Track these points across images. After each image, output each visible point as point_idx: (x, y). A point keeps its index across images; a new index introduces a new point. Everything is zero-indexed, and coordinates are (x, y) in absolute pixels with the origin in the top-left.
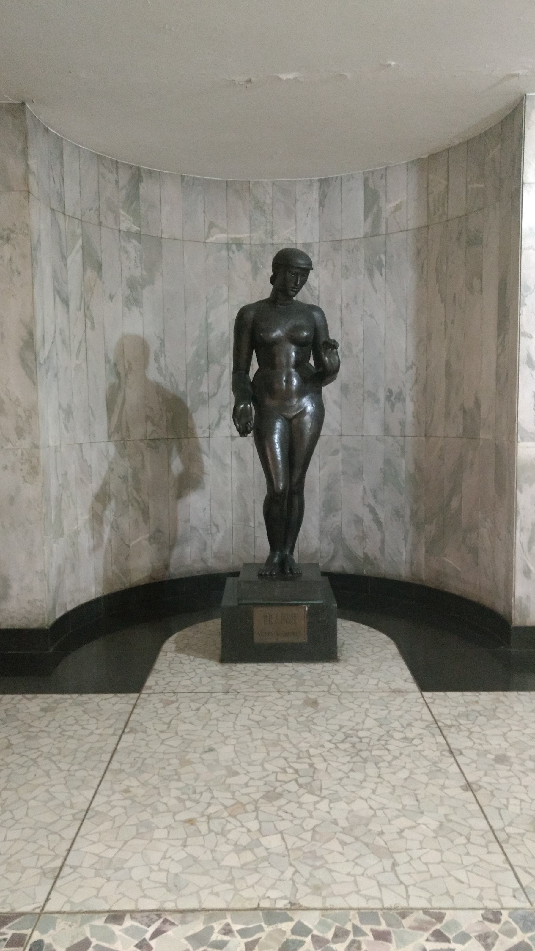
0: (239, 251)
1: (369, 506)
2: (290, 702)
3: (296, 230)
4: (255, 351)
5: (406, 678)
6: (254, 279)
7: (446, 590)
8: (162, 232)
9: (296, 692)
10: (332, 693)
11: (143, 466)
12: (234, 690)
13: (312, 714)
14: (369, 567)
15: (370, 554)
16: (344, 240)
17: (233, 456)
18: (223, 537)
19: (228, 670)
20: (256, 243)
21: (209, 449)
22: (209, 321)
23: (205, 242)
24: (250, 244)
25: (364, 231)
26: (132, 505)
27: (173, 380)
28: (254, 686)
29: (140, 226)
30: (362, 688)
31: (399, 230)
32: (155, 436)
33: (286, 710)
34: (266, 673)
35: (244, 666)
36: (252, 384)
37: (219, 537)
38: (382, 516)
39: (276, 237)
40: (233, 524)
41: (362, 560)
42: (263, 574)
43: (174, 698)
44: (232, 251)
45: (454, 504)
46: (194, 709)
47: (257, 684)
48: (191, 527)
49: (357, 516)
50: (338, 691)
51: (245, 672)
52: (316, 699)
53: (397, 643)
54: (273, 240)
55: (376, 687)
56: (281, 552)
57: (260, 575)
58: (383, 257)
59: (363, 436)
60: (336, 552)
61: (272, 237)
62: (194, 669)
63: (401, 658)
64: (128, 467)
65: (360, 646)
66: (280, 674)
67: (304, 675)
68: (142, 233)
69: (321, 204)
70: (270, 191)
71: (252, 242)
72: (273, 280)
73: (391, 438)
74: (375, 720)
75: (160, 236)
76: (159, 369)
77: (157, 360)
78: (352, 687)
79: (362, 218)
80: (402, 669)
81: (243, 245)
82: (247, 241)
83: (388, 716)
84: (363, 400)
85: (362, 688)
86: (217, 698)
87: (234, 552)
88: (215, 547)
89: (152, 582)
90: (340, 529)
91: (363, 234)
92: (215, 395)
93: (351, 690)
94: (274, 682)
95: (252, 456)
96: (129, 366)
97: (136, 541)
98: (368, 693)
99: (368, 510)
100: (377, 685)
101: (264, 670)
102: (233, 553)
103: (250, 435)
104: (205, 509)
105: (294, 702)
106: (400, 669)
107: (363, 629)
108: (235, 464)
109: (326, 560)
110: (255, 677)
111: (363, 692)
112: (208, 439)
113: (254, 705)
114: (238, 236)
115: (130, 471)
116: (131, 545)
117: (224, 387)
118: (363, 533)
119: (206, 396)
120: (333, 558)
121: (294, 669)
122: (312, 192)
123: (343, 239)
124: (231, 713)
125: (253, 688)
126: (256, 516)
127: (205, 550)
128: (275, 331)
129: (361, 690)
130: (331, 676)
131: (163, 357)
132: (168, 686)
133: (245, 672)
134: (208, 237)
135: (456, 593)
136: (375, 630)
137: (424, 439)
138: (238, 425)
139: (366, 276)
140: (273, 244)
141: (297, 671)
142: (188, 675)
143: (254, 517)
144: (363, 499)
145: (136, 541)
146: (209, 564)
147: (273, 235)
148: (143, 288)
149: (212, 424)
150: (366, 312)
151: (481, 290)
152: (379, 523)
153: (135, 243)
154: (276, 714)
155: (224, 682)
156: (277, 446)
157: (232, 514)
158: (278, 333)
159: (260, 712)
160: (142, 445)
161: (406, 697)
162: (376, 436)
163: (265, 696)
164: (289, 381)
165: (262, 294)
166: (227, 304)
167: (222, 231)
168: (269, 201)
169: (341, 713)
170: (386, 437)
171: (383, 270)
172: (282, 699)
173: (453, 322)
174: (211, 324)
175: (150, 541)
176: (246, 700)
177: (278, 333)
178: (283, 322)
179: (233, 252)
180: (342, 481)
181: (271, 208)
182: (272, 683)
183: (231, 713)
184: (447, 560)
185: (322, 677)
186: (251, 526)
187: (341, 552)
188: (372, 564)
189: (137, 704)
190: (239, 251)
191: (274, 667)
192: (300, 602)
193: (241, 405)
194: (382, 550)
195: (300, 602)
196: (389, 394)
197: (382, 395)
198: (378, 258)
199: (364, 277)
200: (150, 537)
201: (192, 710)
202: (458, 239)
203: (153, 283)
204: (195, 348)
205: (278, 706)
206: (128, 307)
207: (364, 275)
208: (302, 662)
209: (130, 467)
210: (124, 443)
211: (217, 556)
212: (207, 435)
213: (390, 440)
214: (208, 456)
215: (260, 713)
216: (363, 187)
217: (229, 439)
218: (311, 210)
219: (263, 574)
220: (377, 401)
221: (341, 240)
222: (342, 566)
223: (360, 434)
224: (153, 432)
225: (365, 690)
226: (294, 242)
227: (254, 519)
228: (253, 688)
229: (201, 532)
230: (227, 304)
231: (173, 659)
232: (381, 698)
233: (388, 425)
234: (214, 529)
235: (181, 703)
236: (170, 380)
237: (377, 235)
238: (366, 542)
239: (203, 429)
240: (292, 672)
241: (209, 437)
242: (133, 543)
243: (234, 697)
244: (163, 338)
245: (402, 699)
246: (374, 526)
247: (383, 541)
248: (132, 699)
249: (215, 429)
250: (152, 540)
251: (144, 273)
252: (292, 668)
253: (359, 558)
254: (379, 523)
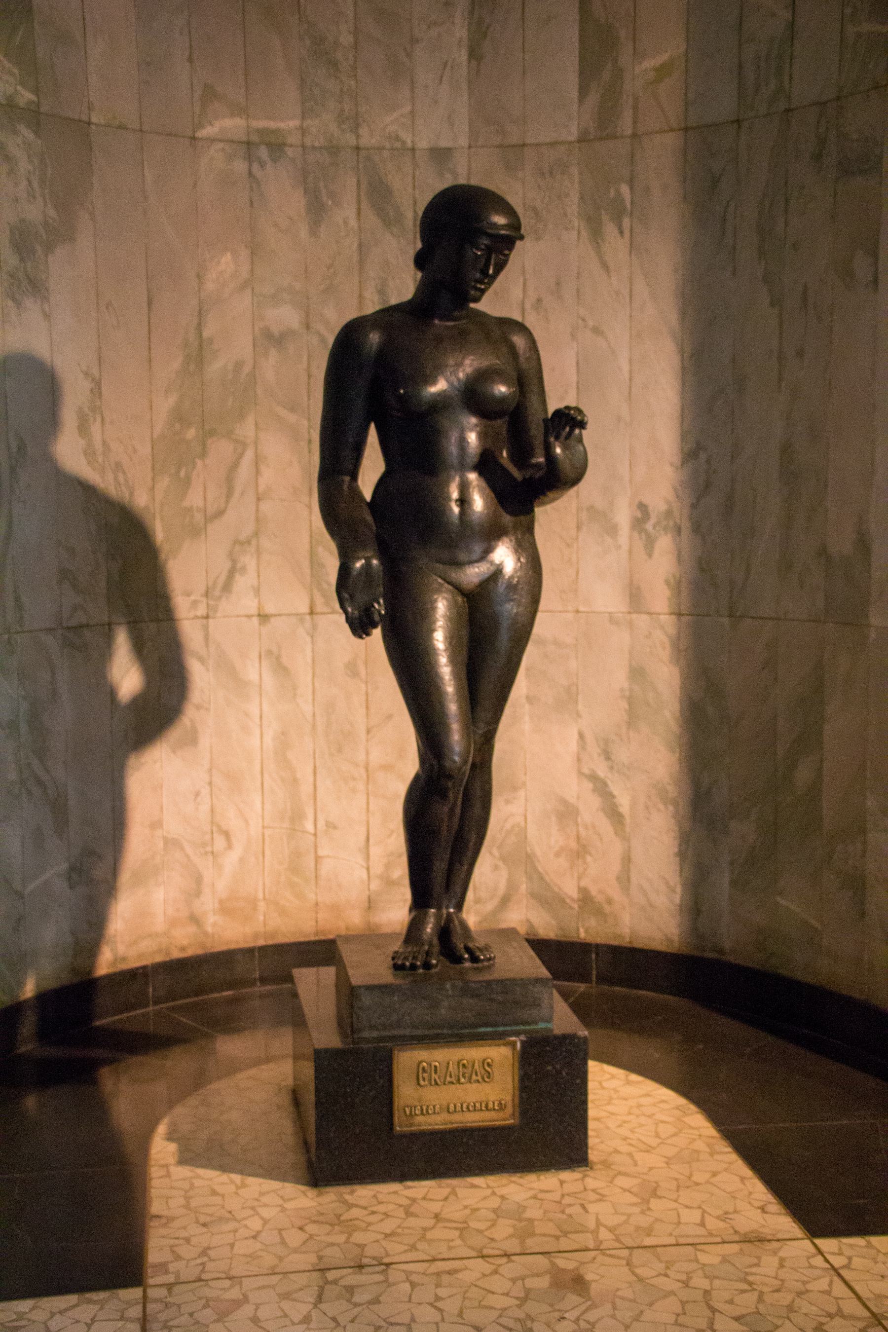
0: (275, 161)
1: (593, 777)
2: (519, 1283)
3: (412, 113)
4: (377, 427)
5: (762, 1203)
6: (314, 231)
7: (784, 972)
8: (91, 107)
9: (524, 1254)
10: (608, 1252)
11: (54, 694)
12: (374, 1258)
13: (584, 1312)
14: (593, 922)
15: (594, 891)
16: (530, 145)
17: (264, 663)
18: (242, 860)
19: (338, 1204)
20: (316, 144)
21: (207, 645)
22: (206, 334)
23: (194, 138)
24: (303, 146)
25: (579, 124)
26: (29, 793)
27: (121, 478)
28: (419, 1246)
29: (36, 91)
30: (671, 1235)
31: (666, 128)
32: (80, 618)
33: (519, 1306)
34: (435, 1207)
35: (372, 1193)
36: (372, 505)
37: (231, 860)
38: (624, 803)
39: (364, 131)
40: (263, 827)
41: (576, 906)
42: (408, 964)
43: (234, 1293)
44: (260, 163)
45: (803, 775)
46: (296, 1320)
47: (423, 1238)
48: (166, 841)
49: (564, 802)
50: (618, 1245)
51: (381, 1208)
52: (577, 1269)
53: (704, 1110)
54: (358, 137)
55: (702, 1232)
56: (439, 908)
57: (397, 968)
58: (625, 189)
59: (577, 611)
60: (512, 887)
61: (355, 129)
62: (253, 1208)
63: (730, 1149)
64: (20, 699)
65: (625, 1122)
66: (466, 1207)
67: (525, 1207)
68: (43, 109)
69: (475, 54)
70: (351, 14)
71: (308, 142)
72: (421, 261)
73: (645, 617)
74: (737, 1319)
75: (84, 118)
76: (89, 453)
77: (83, 428)
78: (649, 1232)
79: (575, 95)
80: (743, 1179)
81: (287, 148)
82: (294, 139)
83: (762, 1308)
84: (579, 528)
85: (671, 1235)
86: (342, 1282)
87: (267, 896)
88: (222, 886)
89: (76, 980)
90: (523, 834)
91: (576, 132)
92: (220, 513)
93: (648, 1241)
94: (461, 1230)
95: (309, 660)
96: (19, 448)
97: (38, 882)
98: (690, 1247)
99: (590, 786)
100: (702, 1224)
101: (424, 1198)
102: (264, 899)
103: (377, 633)
104: (197, 794)
105: (531, 1283)
106: (737, 1179)
107: (613, 1077)
108: (269, 681)
109: (490, 906)
110: (411, 1219)
111: (678, 1245)
112: (204, 621)
113: (438, 1298)
114: (272, 125)
115: (24, 706)
116: (27, 891)
117: (242, 494)
118: (578, 843)
119: (199, 517)
120: (505, 901)
121: (494, 1193)
122: (453, 23)
123: (528, 141)
124: (392, 1324)
125: (417, 1250)
126: (319, 803)
127: (198, 894)
128: (434, 383)
129: (672, 1241)
130: (587, 1206)
131: (99, 419)
132: (205, 1259)
133: (381, 1208)
134: (201, 126)
135: (809, 979)
136: (640, 1078)
137: (725, 621)
138: (350, 610)
139: (584, 233)
140: (357, 148)
141: (503, 1197)
142: (246, 1227)
143: (315, 810)
144: (579, 760)
145: (38, 882)
146: (209, 929)
147: (357, 126)
148: (49, 248)
149: (215, 582)
150: (584, 320)
151: (875, 282)
152: (614, 814)
153: (29, 135)
154: (500, 1316)
155: (341, 1239)
156: (443, 660)
157: (263, 803)
158: (440, 386)
159: (460, 1314)
160: (51, 642)
161: (781, 1254)
162: (610, 613)
163: (456, 1271)
164: (464, 501)
165: (332, 270)
166: (248, 291)
167: (238, 110)
168: (346, 39)
169: (651, 1304)
170: (634, 616)
171: (626, 222)
172: (497, 1276)
173: (800, 354)
174: (211, 341)
175: (69, 879)
176: (413, 1285)
177: (440, 386)
178: (451, 362)
179: (262, 165)
180: (527, 718)
181: (351, 58)
182: (457, 1233)
183: (392, 1324)
184: (783, 902)
185: (568, 1211)
186: (307, 832)
187: (523, 887)
188: (599, 912)
189: (148, 1318)
190: (275, 161)
191: (446, 1191)
192: (501, 1029)
193: (359, 559)
194: (624, 879)
195: (501, 1029)
196: (639, 515)
197: (623, 516)
198: (612, 193)
199: (579, 238)
200: (72, 868)
201: (293, 1324)
202: (818, 157)
203: (72, 239)
204: (172, 400)
205: (496, 1296)
206: (14, 299)
207: (579, 232)
208: (508, 1172)
209: (24, 698)
210: (9, 638)
211: (226, 909)
212: (201, 611)
213: (642, 621)
214: (203, 664)
215: (462, 1317)
216: (576, 16)
217: (255, 620)
218: (448, 68)
219: (408, 964)
220: (612, 530)
221: (524, 145)
222: (528, 921)
223: (570, 608)
224: (75, 608)
225: (682, 1241)
226: (409, 144)
227: (315, 813)
228: (417, 1250)
229: (189, 850)
230: (248, 291)
231: (192, 1186)
232: (725, 1260)
233: (638, 588)
234: (220, 843)
235: (257, 1306)
236: (116, 479)
237: (613, 137)
238: (585, 863)
239: (193, 598)
240: (494, 1202)
241: (207, 617)
242: (31, 887)
243: (379, 1278)
244: (97, 375)
245: (774, 1261)
246: (605, 826)
247: (627, 860)
248: (130, 1304)
249: (220, 598)
250: (75, 876)
251: (52, 212)
252: (489, 1191)
253: (568, 901)
254: (614, 814)
